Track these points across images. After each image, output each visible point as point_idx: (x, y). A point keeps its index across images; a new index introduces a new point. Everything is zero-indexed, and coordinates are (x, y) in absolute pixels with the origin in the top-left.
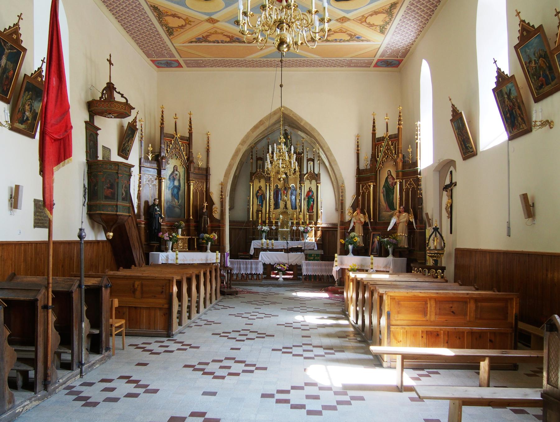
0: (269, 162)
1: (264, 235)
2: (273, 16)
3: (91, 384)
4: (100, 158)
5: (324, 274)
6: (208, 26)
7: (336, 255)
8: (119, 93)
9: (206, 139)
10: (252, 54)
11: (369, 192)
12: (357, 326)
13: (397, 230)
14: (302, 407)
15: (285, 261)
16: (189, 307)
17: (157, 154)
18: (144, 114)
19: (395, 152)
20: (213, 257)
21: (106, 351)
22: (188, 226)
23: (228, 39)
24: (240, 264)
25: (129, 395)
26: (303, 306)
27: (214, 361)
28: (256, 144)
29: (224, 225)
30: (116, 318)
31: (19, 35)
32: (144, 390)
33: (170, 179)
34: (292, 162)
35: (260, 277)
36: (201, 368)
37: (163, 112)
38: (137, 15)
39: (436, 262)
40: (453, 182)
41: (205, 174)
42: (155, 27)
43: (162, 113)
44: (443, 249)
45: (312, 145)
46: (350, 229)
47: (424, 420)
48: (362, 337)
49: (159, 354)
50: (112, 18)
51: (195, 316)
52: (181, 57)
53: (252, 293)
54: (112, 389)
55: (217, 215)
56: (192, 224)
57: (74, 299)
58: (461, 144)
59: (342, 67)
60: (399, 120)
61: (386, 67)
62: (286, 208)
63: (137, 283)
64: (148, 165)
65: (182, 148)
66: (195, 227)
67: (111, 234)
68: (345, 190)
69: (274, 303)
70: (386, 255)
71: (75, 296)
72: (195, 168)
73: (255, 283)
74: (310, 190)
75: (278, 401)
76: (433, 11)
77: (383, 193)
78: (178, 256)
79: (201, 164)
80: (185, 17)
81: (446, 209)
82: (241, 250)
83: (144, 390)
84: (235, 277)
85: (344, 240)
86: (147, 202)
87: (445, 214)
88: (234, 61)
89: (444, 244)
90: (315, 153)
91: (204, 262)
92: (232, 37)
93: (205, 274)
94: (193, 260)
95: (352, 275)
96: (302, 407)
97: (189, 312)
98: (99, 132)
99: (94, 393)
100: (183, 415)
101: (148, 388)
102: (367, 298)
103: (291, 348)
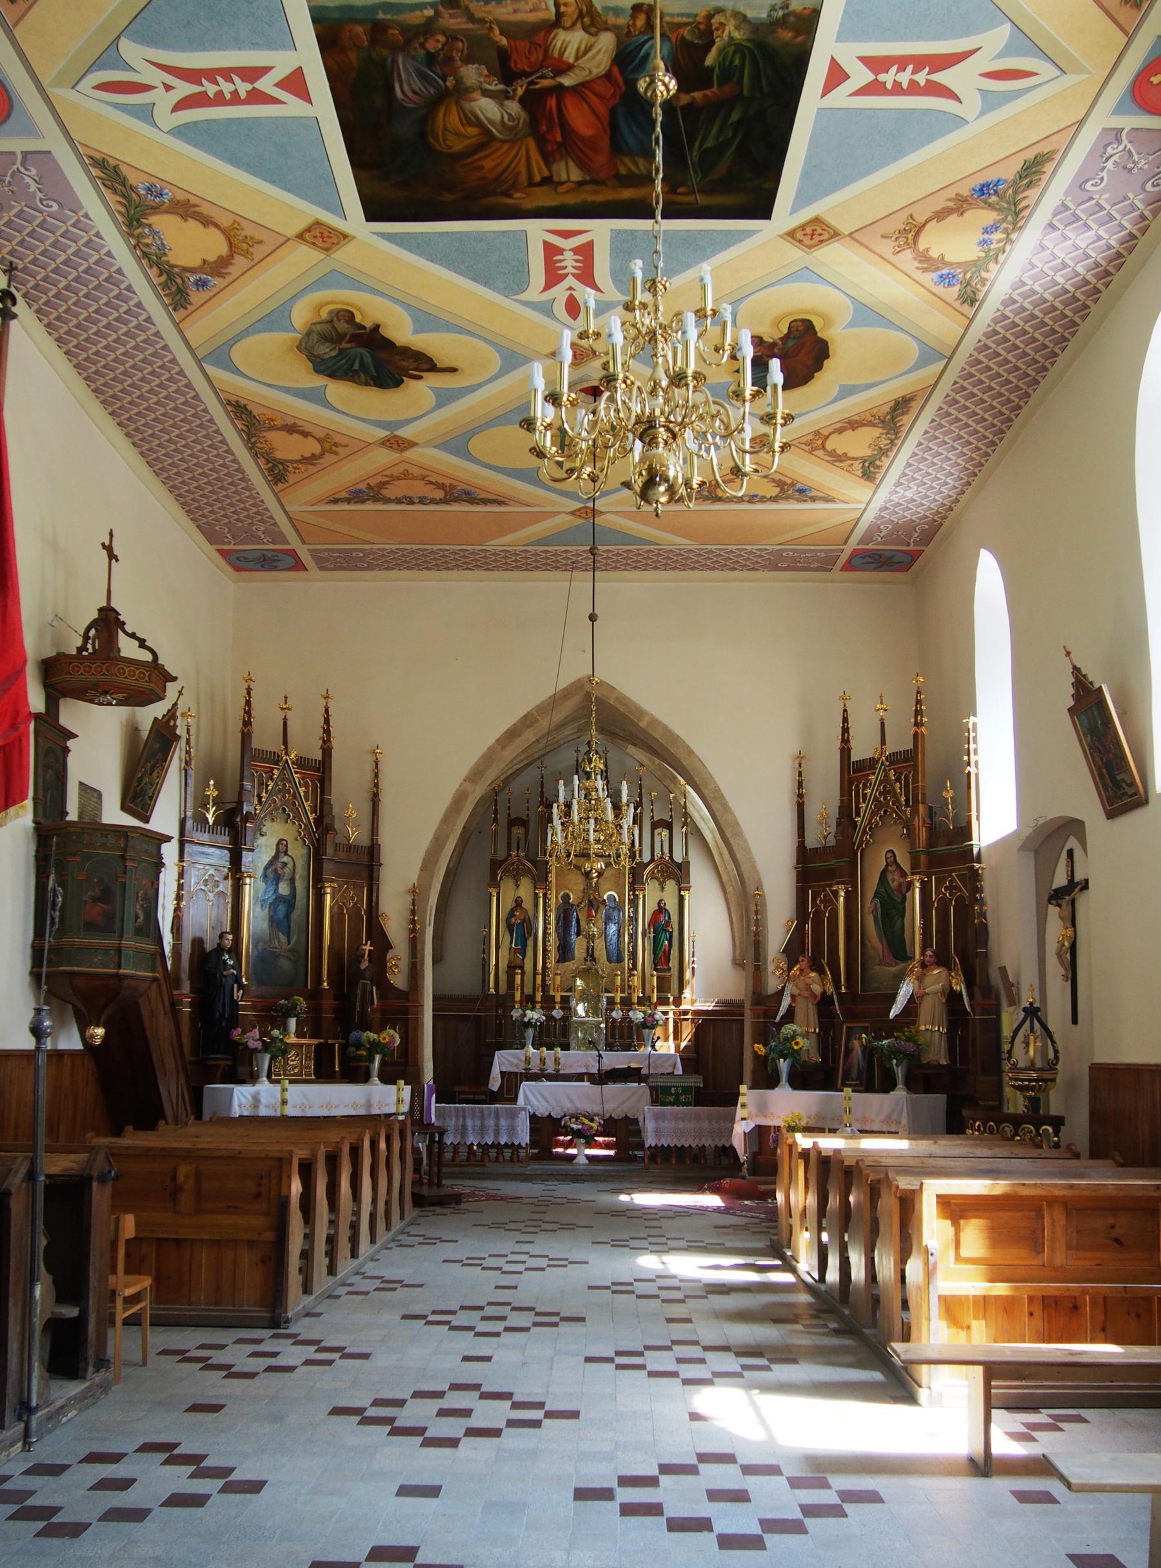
0: (559, 828)
1: (530, 1033)
2: (632, 405)
3: (57, 1470)
4: (73, 815)
5: (707, 1142)
6: (385, 458)
7: (743, 1088)
8: (133, 636)
9: (369, 767)
10: (503, 534)
11: (835, 912)
12: (823, 1287)
13: (917, 1015)
14: (703, 1525)
15: (594, 1108)
16: (331, 1240)
17: (228, 806)
18: (197, 699)
19: (907, 800)
20: (387, 1098)
21: (97, 1371)
22: (315, 1009)
23: (440, 494)
24: (464, 1118)
25: (178, 1500)
26: (656, 1230)
27: (417, 1395)
28: (507, 780)
29: (420, 1006)
30: (128, 1271)
32: (220, 1483)
33: (265, 876)
34: (625, 827)
35: (522, 1153)
36: (382, 1416)
37: (249, 690)
38: (187, 427)
39: (1034, 1103)
40: (1077, 879)
41: (366, 864)
42: (235, 461)
43: (249, 693)
44: (1052, 1066)
45: (667, 782)
46: (781, 1013)
47: (1073, 1557)
48: (842, 1318)
49: (251, 1375)
50: (117, 435)
51: (346, 1265)
52: (304, 542)
53: (502, 1199)
54: (125, 1484)
55: (398, 979)
56: (328, 1002)
57: (13, 1214)
58: (1101, 775)
59: (755, 569)
60: (918, 713)
61: (875, 570)
62: (594, 959)
63: (184, 1170)
64: (205, 837)
65: (302, 790)
67: (100, 1031)
68: (764, 905)
69: (571, 1227)
70: (888, 1086)
71: (17, 1206)
72: (337, 847)
73: (509, 1170)
74: (661, 909)
75: (628, 1510)
76: (1010, 420)
77: (874, 912)
78: (287, 1095)
79: (356, 835)
80: (320, 434)
81: (1059, 955)
82: (464, 1079)
83: (220, 1483)
84: (448, 1155)
85: (765, 1045)
86: (198, 943)
87: (1055, 970)
88: (453, 553)
89: (1056, 1052)
90: (672, 806)
91: (362, 1112)
92: (452, 487)
93: (374, 1145)
94: (329, 1105)
95: (804, 1142)
96: (703, 1525)
97: (331, 1253)
98: (71, 744)
99: (71, 1494)
100: (357, 1560)
101: (232, 1477)
102: (858, 1203)
103: (640, 1354)
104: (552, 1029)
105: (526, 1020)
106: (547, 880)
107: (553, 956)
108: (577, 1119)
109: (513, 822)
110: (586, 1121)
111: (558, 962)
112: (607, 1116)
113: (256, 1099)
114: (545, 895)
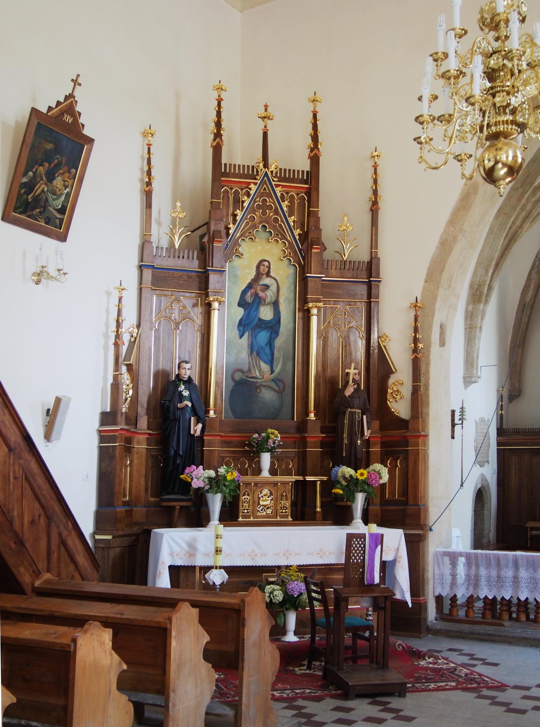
24: (477, 567)
31: (76, 115)
56: (315, 435)
66: (323, 444)
79: (356, 250)
113: (192, 548)
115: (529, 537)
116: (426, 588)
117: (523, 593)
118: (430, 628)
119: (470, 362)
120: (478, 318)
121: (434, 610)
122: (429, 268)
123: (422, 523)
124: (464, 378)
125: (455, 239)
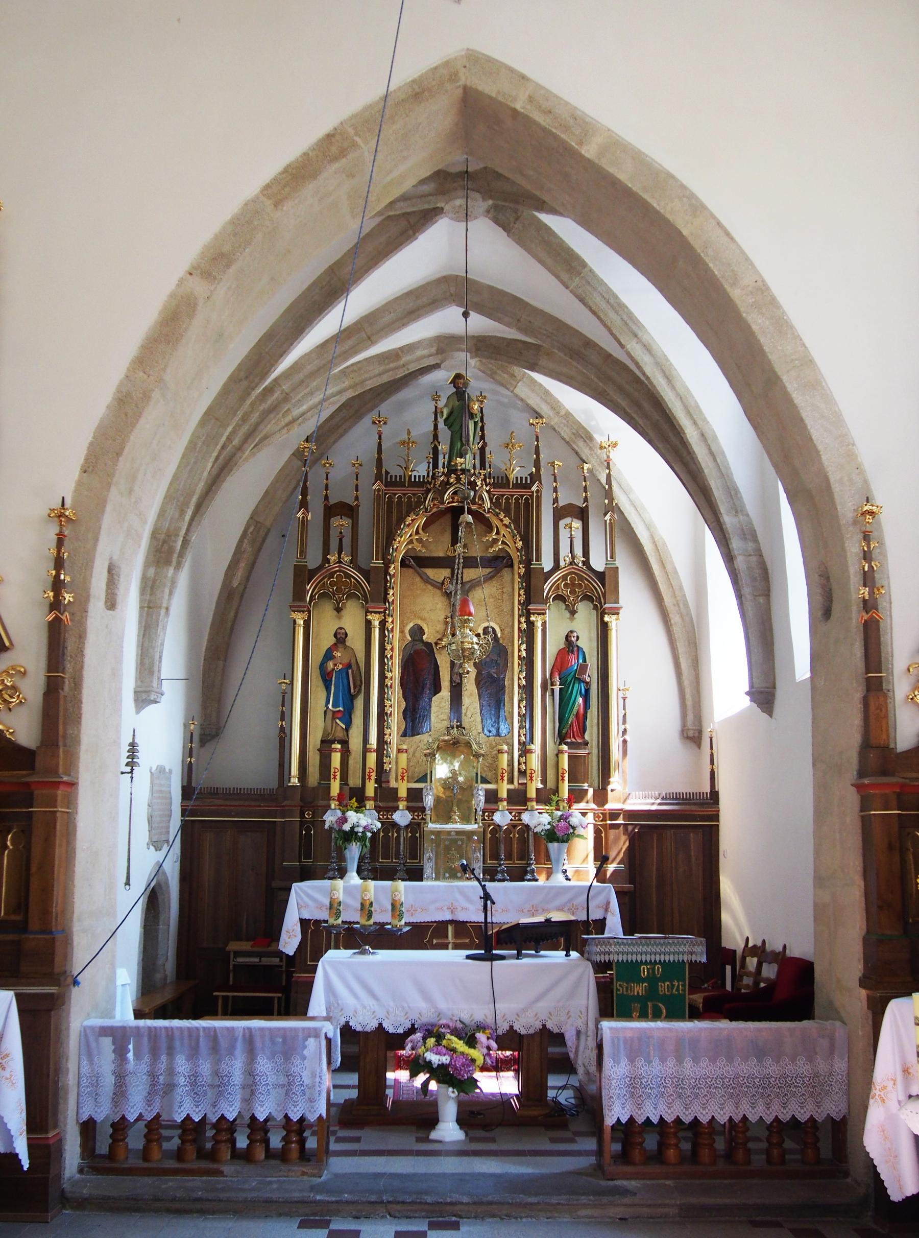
1: (354, 851)
15: (471, 1010)
74: (570, 645)
104: (393, 844)
105: (347, 827)
106: (385, 600)
107: (395, 723)
108: (440, 1037)
109: (332, 510)
110: (460, 1046)
111: (404, 735)
112: (503, 1028)
114: (383, 624)
115: (231, 967)
116: (61, 1107)
117: (262, 1106)
118: (69, 1195)
119: (147, 665)
120: (163, 591)
121: (78, 1150)
122: (91, 444)
123: (56, 970)
124: (135, 692)
125: (147, 396)
